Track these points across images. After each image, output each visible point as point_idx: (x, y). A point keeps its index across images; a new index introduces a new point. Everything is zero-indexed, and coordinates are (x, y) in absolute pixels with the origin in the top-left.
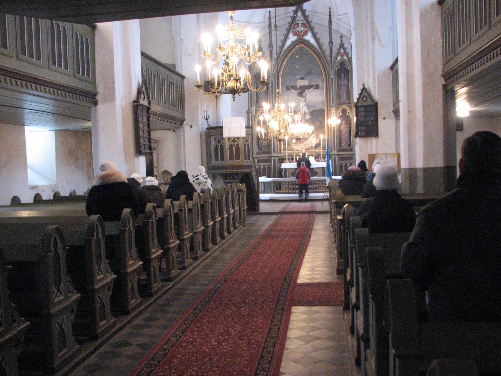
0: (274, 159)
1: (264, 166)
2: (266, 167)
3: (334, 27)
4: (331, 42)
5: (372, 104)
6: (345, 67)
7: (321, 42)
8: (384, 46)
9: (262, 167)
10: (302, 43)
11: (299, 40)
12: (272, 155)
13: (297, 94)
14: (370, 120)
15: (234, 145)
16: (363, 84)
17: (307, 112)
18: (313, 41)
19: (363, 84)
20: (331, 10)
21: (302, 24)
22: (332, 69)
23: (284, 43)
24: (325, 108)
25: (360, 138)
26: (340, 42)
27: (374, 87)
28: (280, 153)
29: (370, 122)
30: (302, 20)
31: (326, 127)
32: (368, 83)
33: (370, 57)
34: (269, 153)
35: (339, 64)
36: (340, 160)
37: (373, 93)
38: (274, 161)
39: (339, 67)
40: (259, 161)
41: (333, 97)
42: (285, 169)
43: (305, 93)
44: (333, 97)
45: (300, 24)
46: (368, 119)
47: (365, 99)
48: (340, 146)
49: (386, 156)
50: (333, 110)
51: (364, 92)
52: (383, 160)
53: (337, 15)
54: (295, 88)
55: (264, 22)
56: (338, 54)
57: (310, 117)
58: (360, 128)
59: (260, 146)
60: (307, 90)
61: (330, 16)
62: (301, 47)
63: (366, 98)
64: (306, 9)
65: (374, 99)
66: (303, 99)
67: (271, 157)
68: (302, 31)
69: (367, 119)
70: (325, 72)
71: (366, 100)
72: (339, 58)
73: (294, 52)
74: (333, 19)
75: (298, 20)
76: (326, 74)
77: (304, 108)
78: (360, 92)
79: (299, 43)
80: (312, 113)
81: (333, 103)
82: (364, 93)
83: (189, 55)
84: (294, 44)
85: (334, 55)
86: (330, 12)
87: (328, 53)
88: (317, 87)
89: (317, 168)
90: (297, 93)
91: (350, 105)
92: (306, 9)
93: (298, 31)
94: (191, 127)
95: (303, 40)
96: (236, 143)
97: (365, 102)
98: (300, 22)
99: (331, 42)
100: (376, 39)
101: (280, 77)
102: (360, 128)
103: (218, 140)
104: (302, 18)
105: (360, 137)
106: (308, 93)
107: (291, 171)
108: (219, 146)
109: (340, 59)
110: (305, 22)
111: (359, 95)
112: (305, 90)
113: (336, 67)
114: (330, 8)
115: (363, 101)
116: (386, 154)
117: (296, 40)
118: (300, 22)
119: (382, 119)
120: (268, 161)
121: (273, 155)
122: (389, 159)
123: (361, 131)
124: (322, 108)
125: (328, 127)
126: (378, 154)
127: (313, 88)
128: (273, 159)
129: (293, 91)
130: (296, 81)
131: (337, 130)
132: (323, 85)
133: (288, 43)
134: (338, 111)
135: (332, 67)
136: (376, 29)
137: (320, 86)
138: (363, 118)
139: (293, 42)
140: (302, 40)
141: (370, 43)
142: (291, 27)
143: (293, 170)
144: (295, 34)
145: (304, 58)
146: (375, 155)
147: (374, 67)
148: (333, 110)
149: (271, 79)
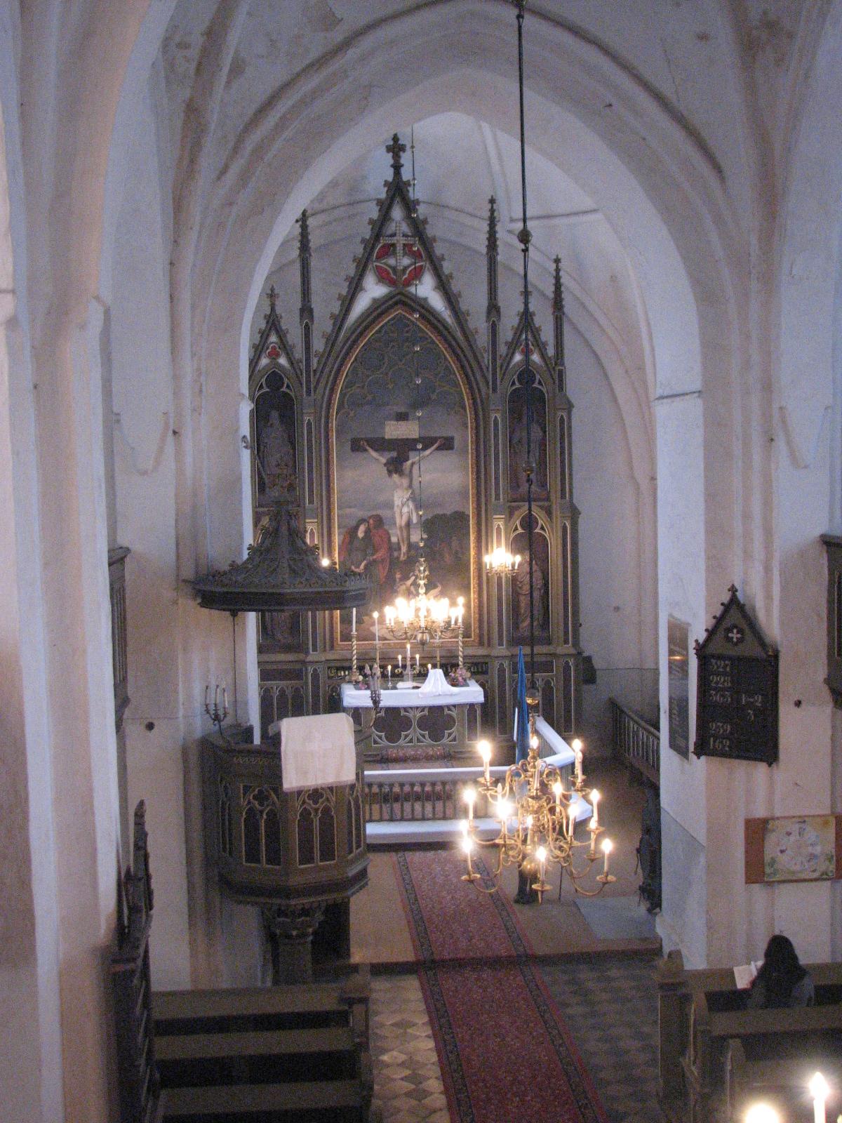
0: (315, 670)
1: (282, 692)
2: (289, 692)
4: (493, 309)
6: (536, 385)
7: (464, 306)
8: (806, 467)
10: (404, 304)
12: (309, 658)
13: (385, 465)
14: (750, 705)
15: (316, 810)
17: (415, 520)
18: (437, 302)
22: (494, 390)
23: (348, 302)
24: (471, 511)
26: (389, 175)
27: (769, 597)
30: (405, 235)
34: (300, 648)
37: (761, 616)
38: (316, 676)
39: (517, 385)
41: (497, 484)
43: (409, 463)
44: (497, 484)
45: (399, 248)
46: (744, 702)
47: (734, 635)
49: (802, 825)
50: (499, 522)
51: (734, 611)
52: (792, 838)
53: (508, 219)
54: (380, 444)
56: (513, 346)
59: (269, 627)
61: (492, 222)
62: (400, 319)
63: (740, 631)
65: (767, 640)
66: (405, 481)
67: (304, 662)
68: (405, 268)
70: (474, 399)
71: (740, 641)
72: (518, 357)
73: (379, 332)
75: (393, 235)
76: (475, 403)
77: (405, 510)
78: (718, 611)
80: (430, 525)
81: (497, 498)
82: (734, 617)
83: (145, 473)
84: (379, 309)
85: (502, 349)
86: (492, 211)
87: (482, 340)
88: (447, 445)
89: (454, 706)
90: (384, 460)
91: (546, 504)
93: (394, 269)
94: (150, 726)
96: (321, 805)
98: (400, 241)
99: (493, 309)
100: (781, 444)
103: (260, 792)
104: (405, 228)
108: (261, 812)
111: (714, 621)
113: (506, 387)
114: (492, 201)
115: (729, 640)
116: (802, 820)
117: (386, 296)
118: (400, 241)
119: (792, 706)
121: (313, 656)
122: (811, 834)
124: (462, 510)
126: (773, 819)
128: (310, 670)
129: (374, 454)
130: (382, 425)
132: (465, 437)
133: (362, 304)
134: (511, 522)
136: (781, 408)
137: (456, 444)
139: (375, 300)
140: (403, 299)
142: (370, 254)
144: (383, 277)
146: (765, 822)
147: (768, 532)
148: (499, 522)
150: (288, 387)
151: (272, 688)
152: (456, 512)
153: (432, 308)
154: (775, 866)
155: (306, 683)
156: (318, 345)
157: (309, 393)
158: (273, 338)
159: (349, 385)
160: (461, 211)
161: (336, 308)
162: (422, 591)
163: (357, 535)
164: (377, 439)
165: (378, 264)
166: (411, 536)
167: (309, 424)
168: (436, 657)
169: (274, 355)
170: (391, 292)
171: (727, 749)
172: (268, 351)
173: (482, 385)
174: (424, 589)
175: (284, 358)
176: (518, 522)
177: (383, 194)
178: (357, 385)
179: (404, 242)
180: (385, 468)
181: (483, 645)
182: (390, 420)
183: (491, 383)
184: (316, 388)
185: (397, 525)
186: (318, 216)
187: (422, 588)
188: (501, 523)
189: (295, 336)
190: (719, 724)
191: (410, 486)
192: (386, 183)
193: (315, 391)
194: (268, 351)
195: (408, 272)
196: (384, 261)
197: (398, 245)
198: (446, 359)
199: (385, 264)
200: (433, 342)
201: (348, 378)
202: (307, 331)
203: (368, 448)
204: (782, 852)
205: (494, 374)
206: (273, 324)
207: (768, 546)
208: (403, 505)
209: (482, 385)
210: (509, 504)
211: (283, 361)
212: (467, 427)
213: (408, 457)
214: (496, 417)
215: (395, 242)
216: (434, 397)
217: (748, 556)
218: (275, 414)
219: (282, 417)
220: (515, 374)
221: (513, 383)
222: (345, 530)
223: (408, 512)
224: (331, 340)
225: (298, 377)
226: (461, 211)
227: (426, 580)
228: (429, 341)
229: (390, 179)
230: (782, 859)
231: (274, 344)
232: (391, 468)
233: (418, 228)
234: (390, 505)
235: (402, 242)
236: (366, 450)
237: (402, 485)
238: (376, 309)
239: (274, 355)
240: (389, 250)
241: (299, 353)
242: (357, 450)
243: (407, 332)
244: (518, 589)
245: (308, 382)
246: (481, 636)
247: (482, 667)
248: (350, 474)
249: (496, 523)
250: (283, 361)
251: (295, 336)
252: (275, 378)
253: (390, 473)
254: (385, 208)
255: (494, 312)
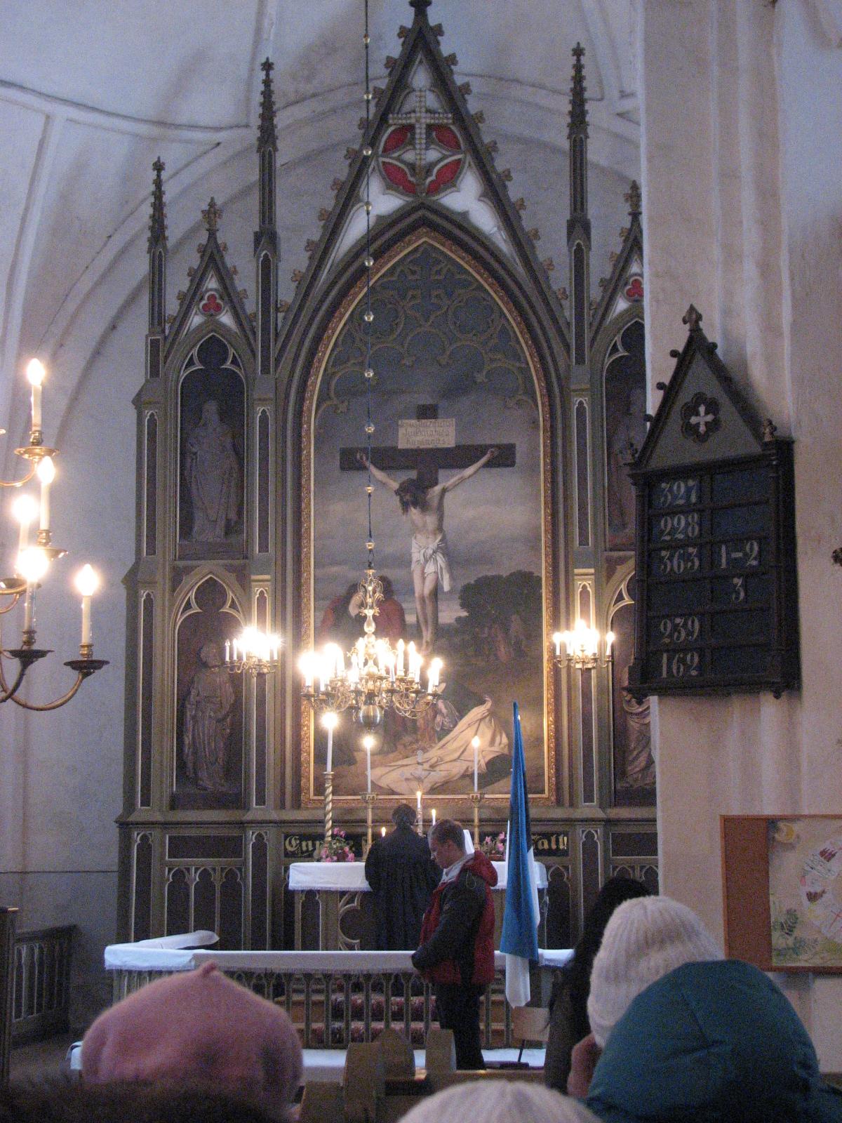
0: (144, 838)
1: (205, 875)
2: (217, 880)
3: (596, 152)
4: (579, 225)
5: (756, 449)
7: (527, 222)
9: (194, 878)
10: (434, 227)
11: (415, 209)
12: (249, 816)
13: (397, 492)
16: (692, 309)
17: (446, 587)
18: (485, 219)
19: (692, 309)
20: (584, 60)
21: (430, 127)
22: (580, 360)
23: (335, 223)
25: (671, 702)
27: (770, 328)
28: (297, 804)
29: (738, 581)
31: (546, 666)
32: (727, 313)
33: (744, 125)
34: (238, 801)
35: (618, 338)
36: (616, 853)
37: (758, 373)
38: (260, 848)
40: (179, 846)
41: (582, 507)
42: (310, 894)
43: (437, 489)
45: (420, 132)
47: (702, 419)
48: (621, 773)
50: (584, 580)
51: (699, 368)
53: (616, 94)
54: (389, 459)
55: (247, 126)
57: (464, 614)
58: (666, 627)
60: (448, 472)
62: (428, 251)
63: (713, 407)
64: (440, 26)
66: (431, 520)
67: (242, 825)
69: (714, 562)
71: (713, 426)
74: (595, 114)
79: (413, 228)
80: (473, 595)
81: (584, 541)
85: (595, 293)
86: (578, 68)
87: (561, 278)
88: (503, 457)
90: (395, 485)
92: (440, 26)
93: (412, 167)
95: (435, 212)
97: (702, 439)
98: (422, 121)
99: (579, 225)
101: (312, 403)
102: (666, 627)
104: (432, 100)
105: (665, 691)
106: (455, 485)
107: (342, 908)
109: (626, 311)
110: (447, 119)
112: (442, 474)
114: (578, 52)
115: (690, 430)
118: (422, 121)
120: (229, 846)
121: (256, 812)
123: (673, 650)
124: (524, 568)
125: (556, 671)
127: (484, 460)
128: (251, 836)
130: (394, 429)
131: (601, 690)
133: (357, 228)
135: (580, 348)
138: (687, 558)
141: (744, 34)
143: (351, 901)
144: (394, 180)
145: (440, 308)
146: (771, 823)
147: (768, 193)
148: (584, 580)
149: (260, 409)
150: (234, 362)
151: (188, 870)
152: (520, 572)
153: (477, 229)
154: (797, 933)
155: (245, 863)
156: (286, 292)
157: (265, 369)
158: (212, 284)
159: (337, 361)
160: (542, 87)
161: (315, 233)
162: (370, 628)
163: (346, 608)
164: (387, 450)
165: (387, 160)
166: (440, 614)
167: (264, 419)
168: (473, 821)
169: (212, 309)
170: (408, 203)
171: (694, 673)
172: (204, 302)
173: (558, 347)
174: (373, 624)
175: (229, 313)
176: (623, 586)
177: (395, 48)
178: (352, 362)
179: (428, 121)
180: (398, 498)
181: (563, 805)
182: (411, 418)
183: (573, 347)
184: (278, 361)
185: (417, 595)
186: (306, 103)
187: (369, 625)
188: (589, 583)
189: (247, 280)
190: (678, 620)
191: (440, 528)
192: (403, 32)
193: (277, 366)
194: (204, 302)
195: (435, 170)
196: (396, 155)
197: (417, 126)
198: (502, 314)
199: (398, 159)
200: (480, 288)
201: (338, 350)
202: (267, 271)
203: (368, 464)
204: (812, 897)
205: (579, 335)
206: (212, 258)
207: (768, 222)
208: (426, 561)
209: (558, 347)
210: (607, 554)
211: (226, 319)
212: (537, 427)
213: (437, 479)
214: (581, 403)
215: (413, 121)
216: (480, 378)
217: (732, 256)
218: (211, 408)
219: (224, 415)
220: (618, 332)
221: (615, 349)
222: (327, 603)
223: (436, 573)
224: (307, 283)
225: (250, 344)
226: (542, 87)
227: (377, 610)
228: (474, 286)
229: (409, 24)
230: (816, 914)
231: (212, 293)
232: (408, 497)
233: (451, 94)
234: (404, 561)
235: (423, 120)
236: (365, 468)
237: (425, 525)
238: (381, 233)
239: (212, 309)
240: (404, 135)
241: (252, 305)
242: (350, 469)
243: (438, 272)
244: (625, 706)
245: (266, 348)
246: (558, 788)
247: (557, 841)
248: (338, 508)
249: (579, 584)
250: (226, 319)
251: (247, 280)
252: (213, 348)
253: (405, 506)
254: (400, 71)
255: (578, 229)
